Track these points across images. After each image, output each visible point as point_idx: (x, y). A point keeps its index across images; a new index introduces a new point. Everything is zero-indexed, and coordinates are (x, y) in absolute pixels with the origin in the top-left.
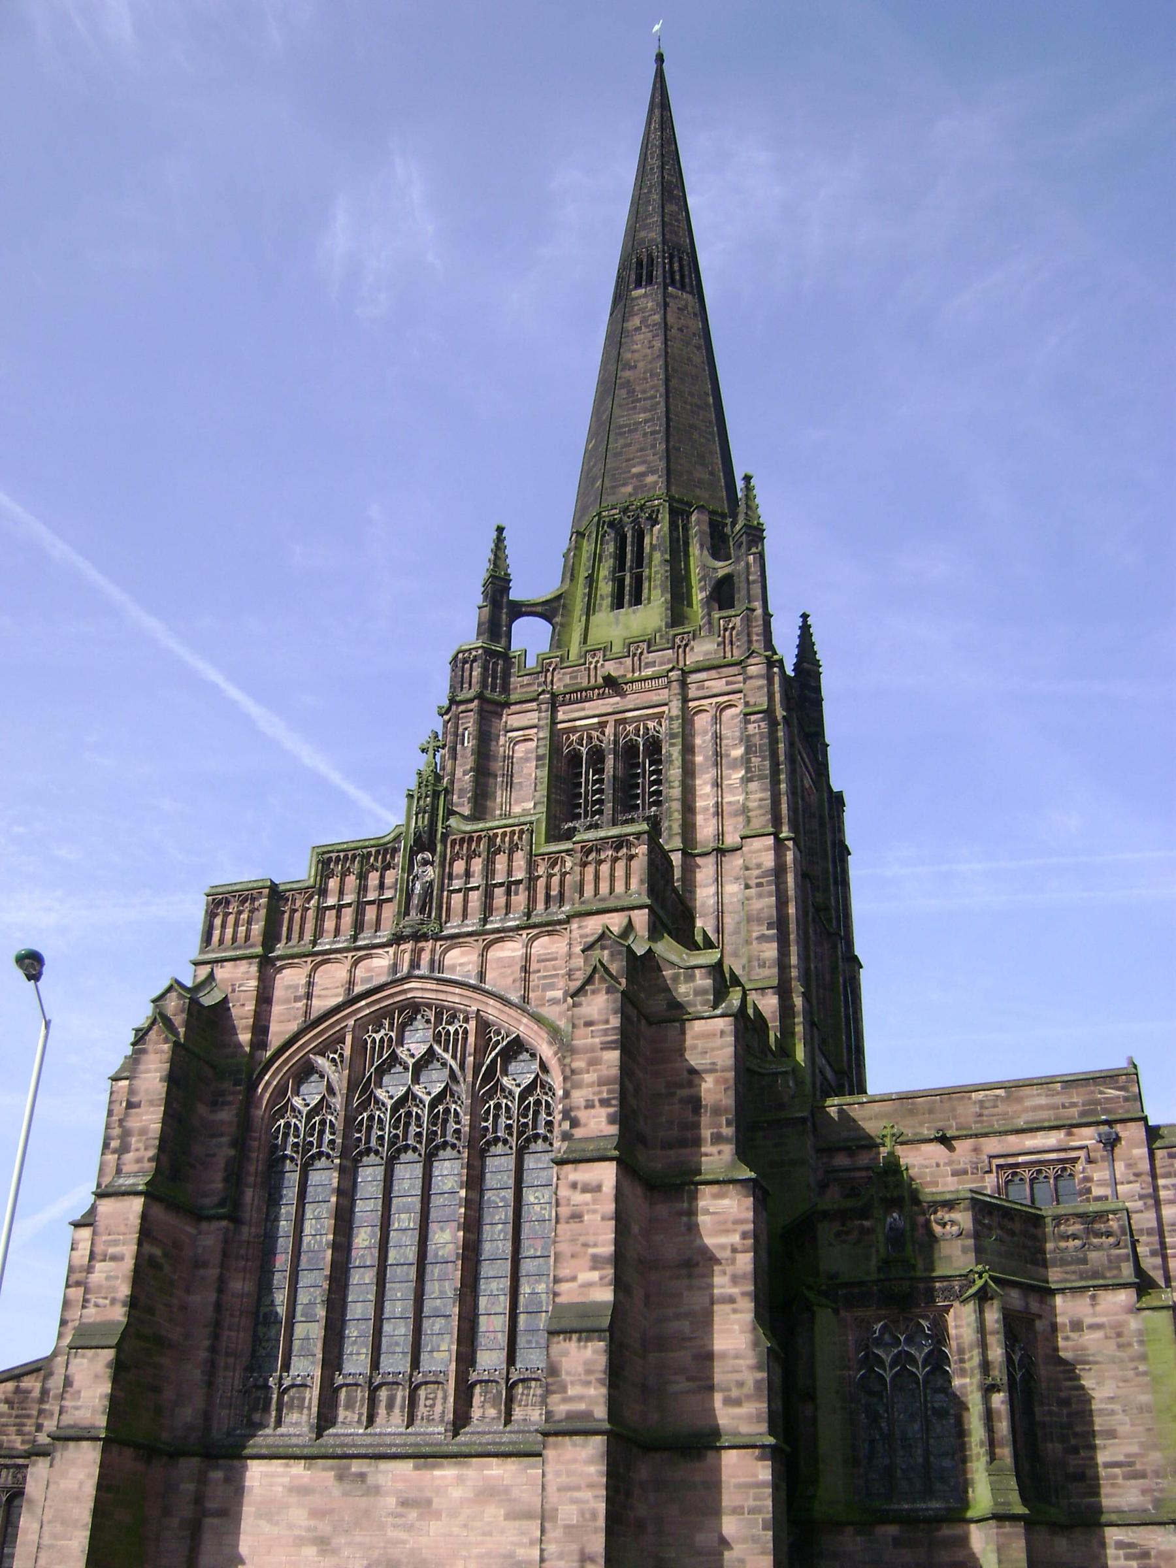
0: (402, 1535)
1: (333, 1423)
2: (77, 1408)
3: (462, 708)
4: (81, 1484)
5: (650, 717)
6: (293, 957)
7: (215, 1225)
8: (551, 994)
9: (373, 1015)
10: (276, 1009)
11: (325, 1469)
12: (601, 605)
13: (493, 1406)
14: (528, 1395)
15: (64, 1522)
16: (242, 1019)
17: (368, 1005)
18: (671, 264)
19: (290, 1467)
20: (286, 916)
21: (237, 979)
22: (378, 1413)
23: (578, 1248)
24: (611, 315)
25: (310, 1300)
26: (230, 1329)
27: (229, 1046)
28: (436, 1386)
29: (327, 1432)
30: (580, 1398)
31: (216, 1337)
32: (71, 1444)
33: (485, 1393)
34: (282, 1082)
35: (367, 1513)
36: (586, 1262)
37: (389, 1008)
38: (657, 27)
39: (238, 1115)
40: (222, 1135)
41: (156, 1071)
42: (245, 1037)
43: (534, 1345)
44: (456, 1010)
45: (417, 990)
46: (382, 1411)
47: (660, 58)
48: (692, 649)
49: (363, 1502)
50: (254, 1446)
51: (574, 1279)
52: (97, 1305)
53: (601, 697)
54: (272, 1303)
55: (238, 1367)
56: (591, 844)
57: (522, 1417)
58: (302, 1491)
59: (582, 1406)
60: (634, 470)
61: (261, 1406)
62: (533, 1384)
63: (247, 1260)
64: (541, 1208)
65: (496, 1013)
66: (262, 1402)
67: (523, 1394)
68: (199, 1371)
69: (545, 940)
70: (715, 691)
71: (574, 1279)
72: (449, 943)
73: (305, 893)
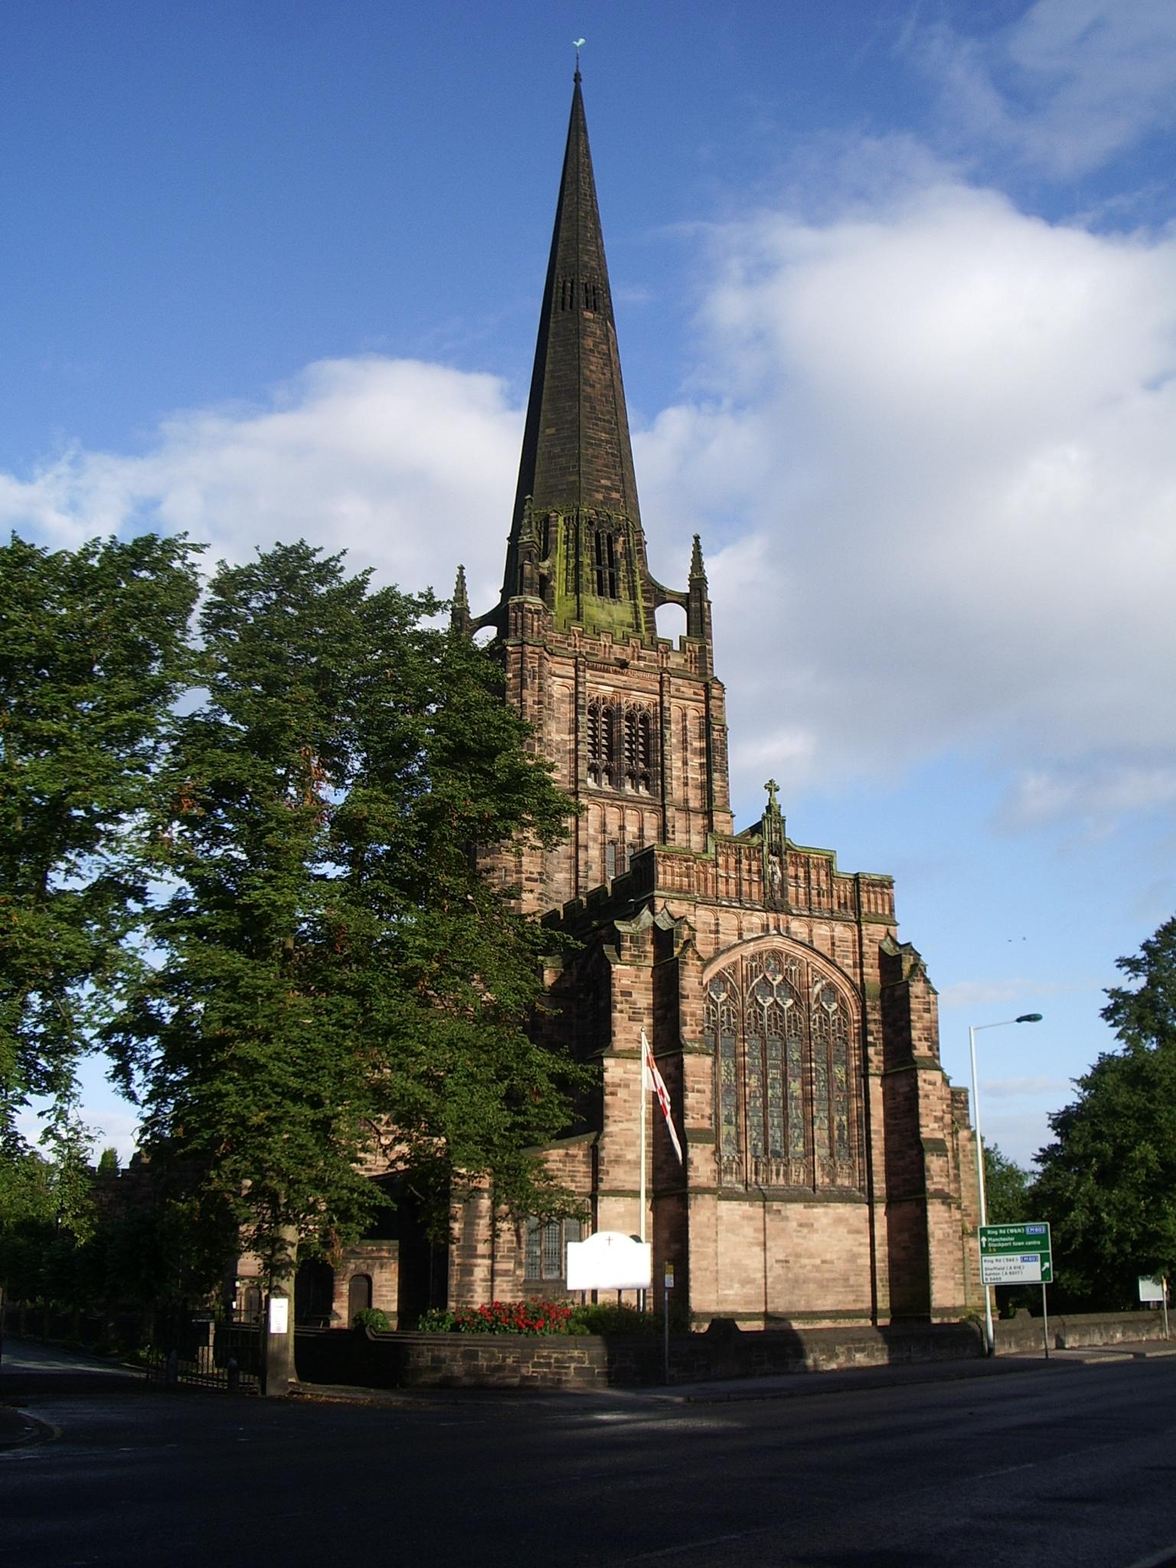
0: (800, 1241)
8: (846, 961)
15: (702, 1239)
30: (939, 1183)
35: (783, 1230)
36: (932, 1119)
47: (577, 78)
49: (782, 1224)
59: (940, 1187)
70: (687, 696)
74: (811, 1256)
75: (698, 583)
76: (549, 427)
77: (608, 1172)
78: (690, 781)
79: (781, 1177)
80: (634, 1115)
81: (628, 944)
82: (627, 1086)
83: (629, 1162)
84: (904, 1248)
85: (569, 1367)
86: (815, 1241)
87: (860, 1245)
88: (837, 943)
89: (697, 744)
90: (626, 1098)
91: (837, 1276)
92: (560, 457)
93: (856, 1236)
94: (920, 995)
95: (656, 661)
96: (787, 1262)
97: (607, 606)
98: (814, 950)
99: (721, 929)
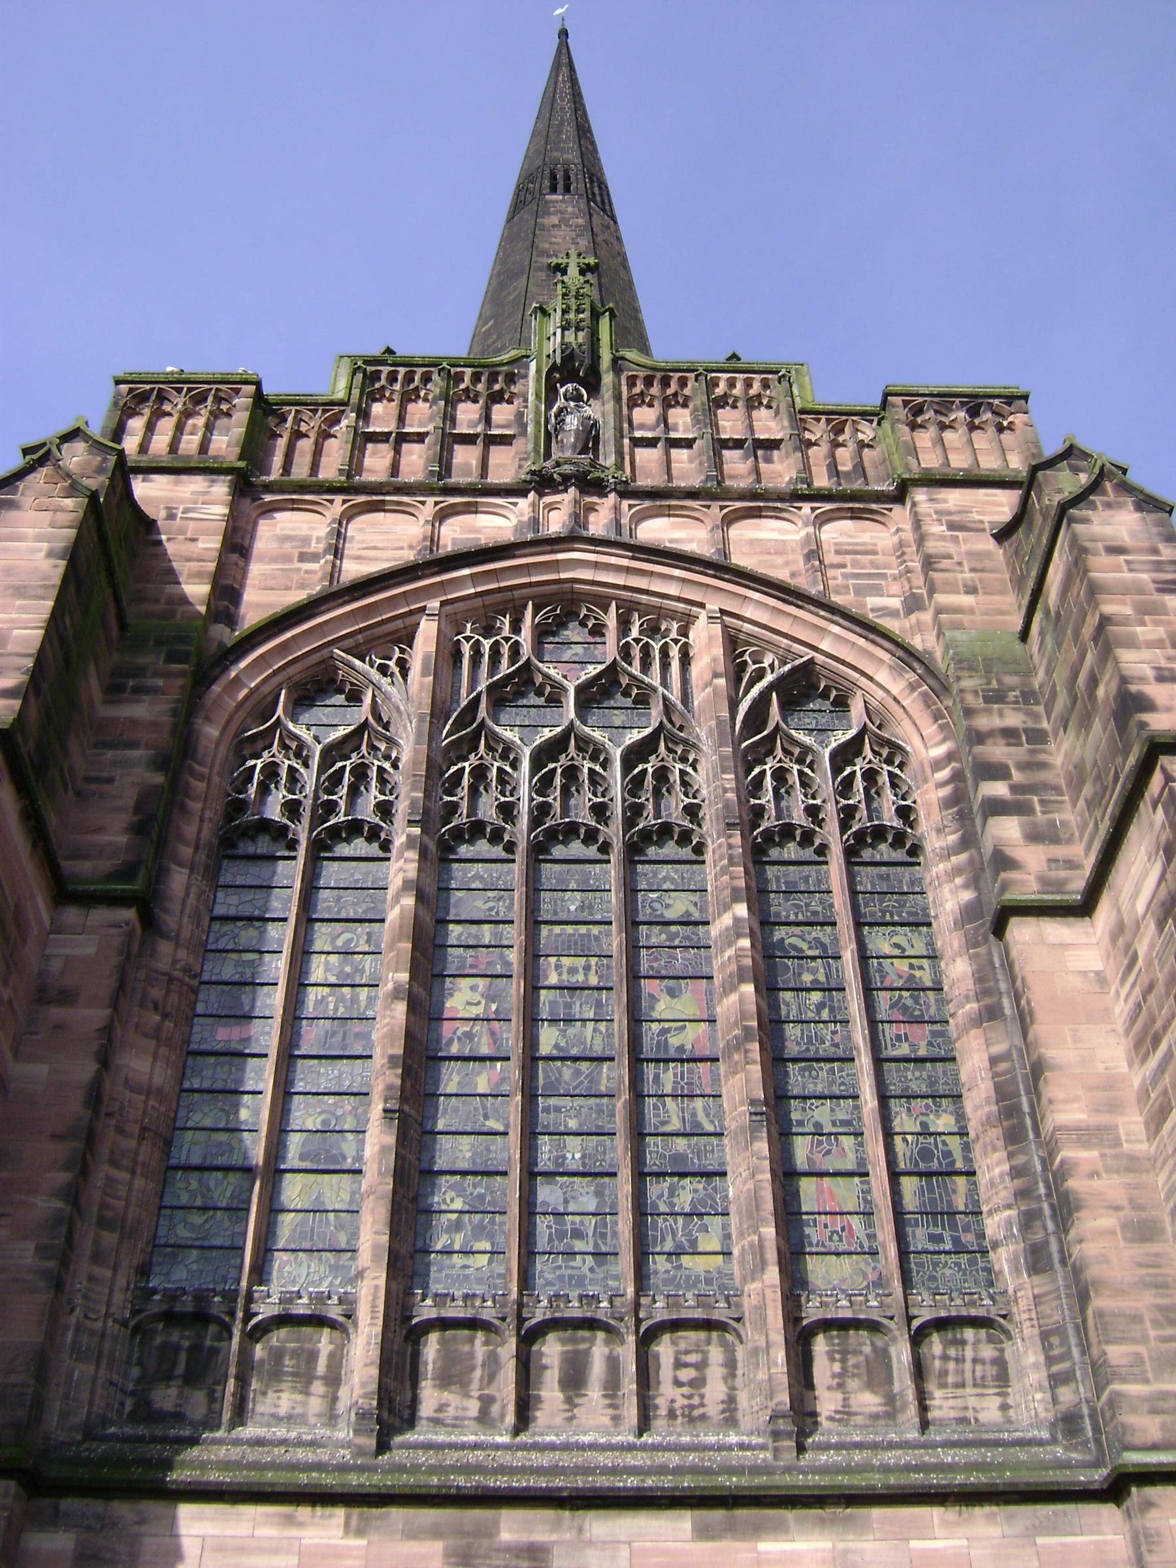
1: (410, 1422)
7: (101, 915)
9: (478, 602)
10: (256, 569)
11: (412, 1534)
13: (870, 1385)
14: (960, 1360)
16: (189, 560)
18: (592, 187)
19: (300, 1525)
20: (281, 444)
21: (182, 501)
22: (539, 1399)
24: (509, 221)
25: (324, 1122)
26: (114, 1163)
27: (157, 600)
28: (702, 1335)
29: (398, 1439)
31: (83, 1167)
34: (266, 689)
37: (517, 594)
38: (559, 11)
39: (174, 712)
40: (133, 745)
41: (38, 538)
42: (197, 591)
43: (948, 1246)
44: (663, 613)
46: (550, 1393)
50: (190, 1464)
55: (125, 1263)
56: (920, 400)
57: (953, 1414)
61: (180, 1369)
62: (969, 1333)
63: (165, 1016)
64: (911, 966)
65: (763, 617)
66: (183, 1357)
67: (945, 1358)
68: (32, 1246)
69: (847, 525)
72: (647, 504)
73: (324, 411)
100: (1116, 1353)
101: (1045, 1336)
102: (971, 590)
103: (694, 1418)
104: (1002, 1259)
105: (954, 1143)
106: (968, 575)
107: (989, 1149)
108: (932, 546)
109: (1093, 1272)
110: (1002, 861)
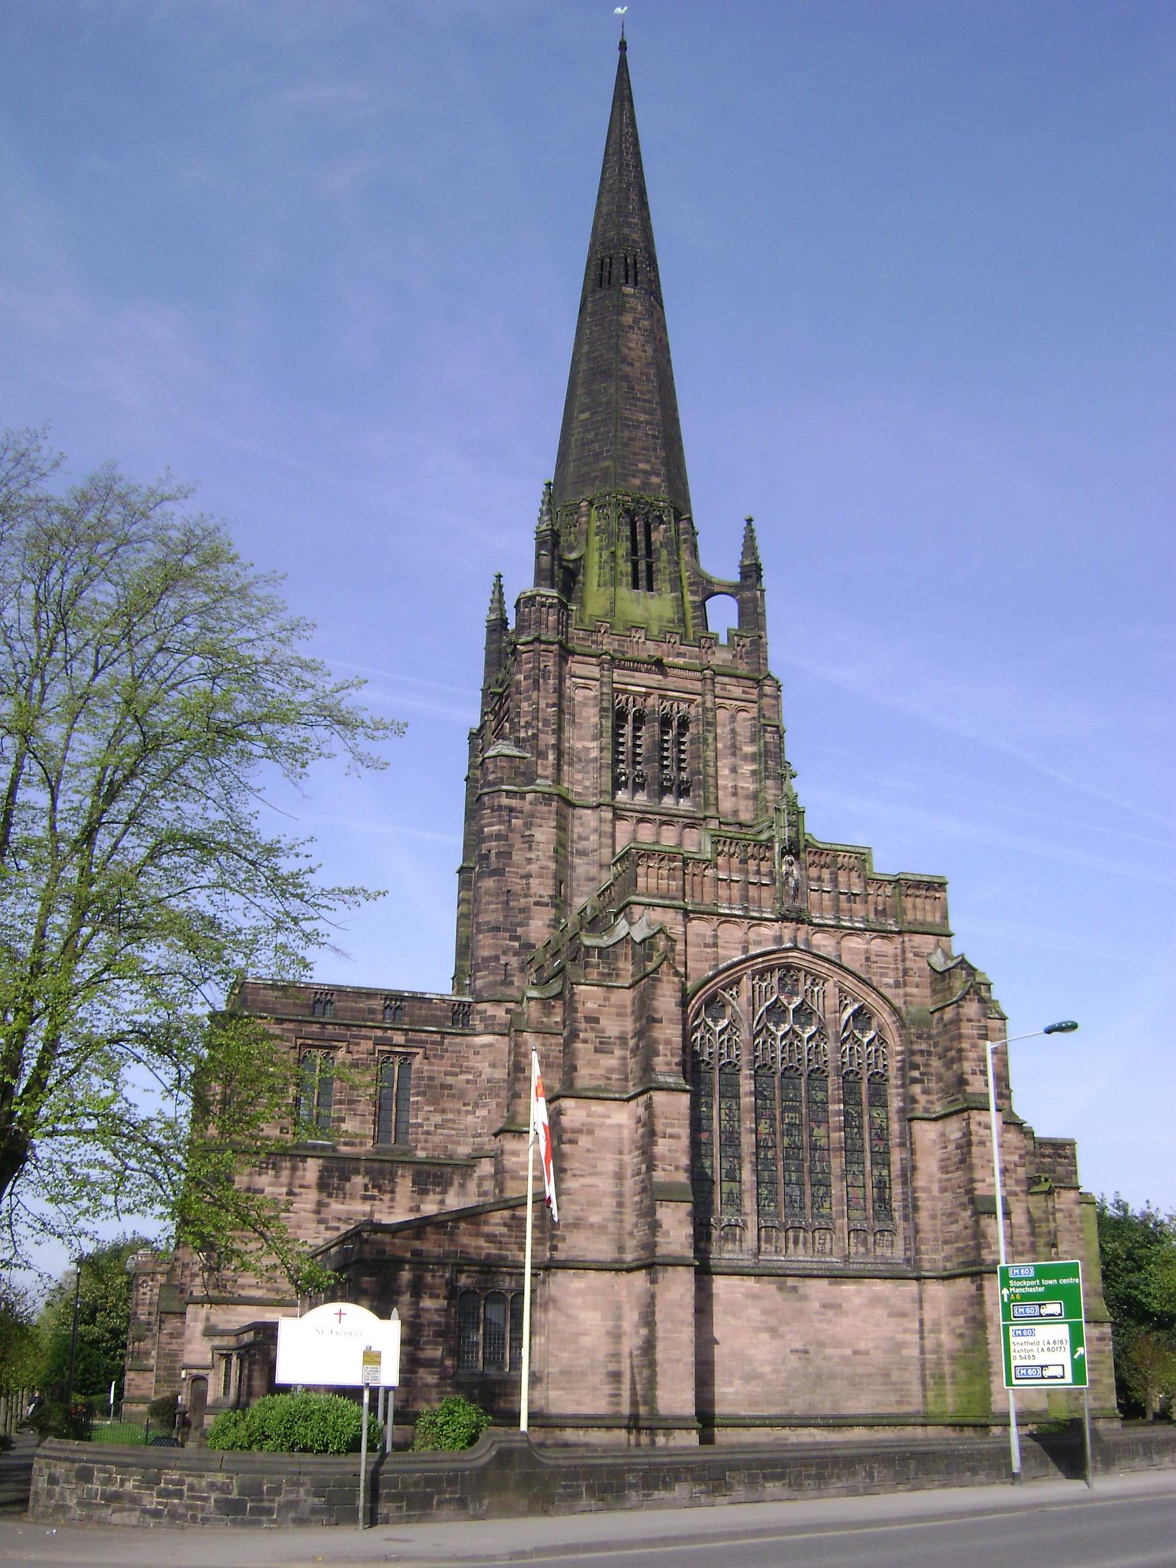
0: (824, 1326)
2: (668, 1243)
3: (543, 647)
4: (682, 1296)
5: (684, 700)
6: (703, 913)
8: (885, 980)
11: (769, 1283)
12: (621, 581)
15: (673, 1321)
17: (763, 962)
23: (985, 1163)
32: (670, 1268)
33: (857, 1237)
38: (618, 10)
41: (672, 997)
45: (795, 958)
46: (791, 1245)
47: (623, 46)
48: (714, 653)
49: (798, 1305)
51: (984, 1181)
52: (664, 1170)
53: (648, 671)
54: (703, 1167)
58: (756, 1297)
60: (642, 466)
69: (878, 941)
71: (984, 1181)
74: (838, 1345)
75: (752, 572)
76: (582, 412)
77: (564, 1239)
78: (739, 790)
79: (801, 1245)
80: (599, 1168)
81: (595, 960)
82: (591, 1132)
83: (592, 1226)
84: (961, 1336)
85: (206, 1499)
86: (844, 1326)
87: (905, 1331)
88: (873, 958)
89: (749, 749)
90: (589, 1146)
91: (873, 1370)
92: (593, 442)
93: (900, 1320)
94: (973, 1016)
95: (697, 658)
96: (806, 1352)
97: (642, 599)
98: (841, 966)
99: (720, 942)
100: (923, 1248)
101: (905, 1238)
102: (917, 986)
103: (823, 1253)
104: (896, 1215)
105: (887, 1179)
106: (917, 979)
107: (715, 839)
108: (908, 964)
109: (921, 1227)
110: (914, 1100)
